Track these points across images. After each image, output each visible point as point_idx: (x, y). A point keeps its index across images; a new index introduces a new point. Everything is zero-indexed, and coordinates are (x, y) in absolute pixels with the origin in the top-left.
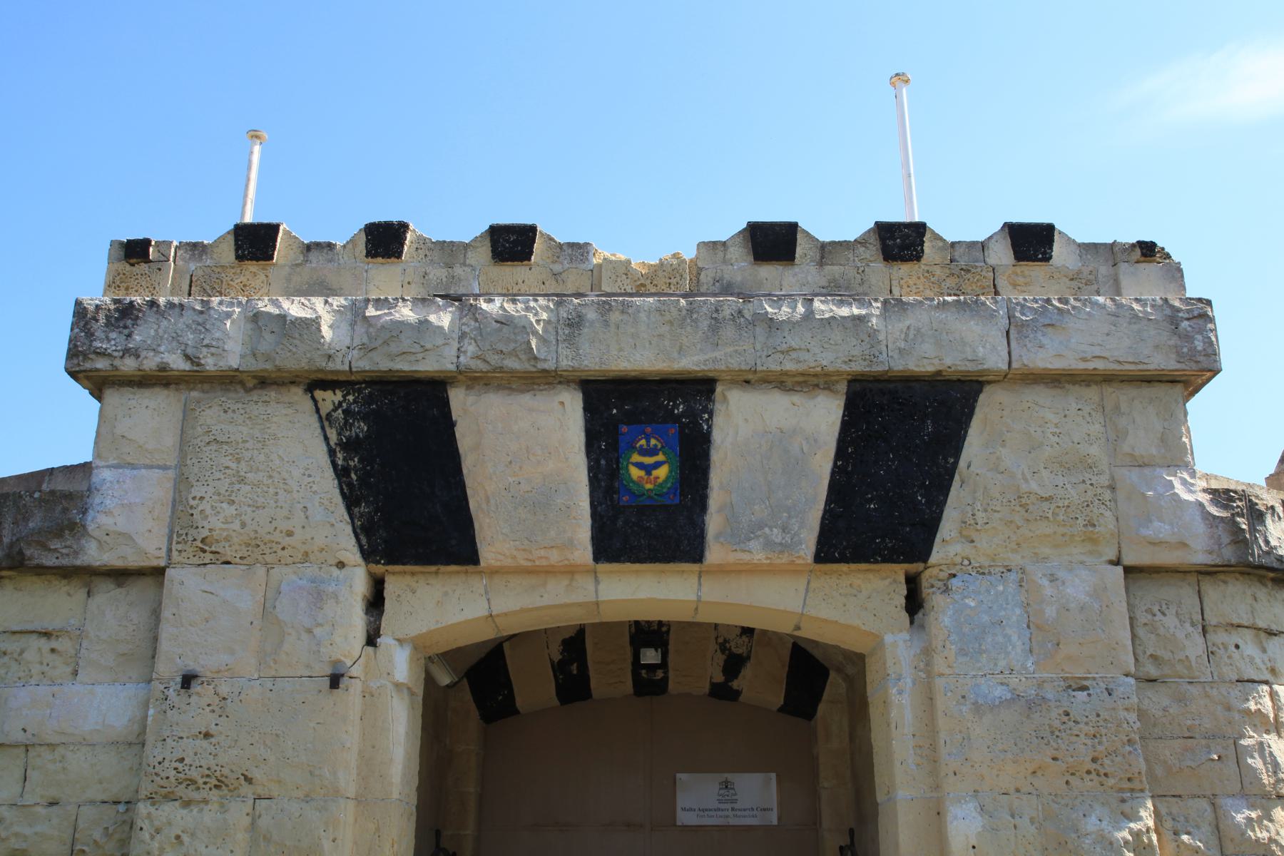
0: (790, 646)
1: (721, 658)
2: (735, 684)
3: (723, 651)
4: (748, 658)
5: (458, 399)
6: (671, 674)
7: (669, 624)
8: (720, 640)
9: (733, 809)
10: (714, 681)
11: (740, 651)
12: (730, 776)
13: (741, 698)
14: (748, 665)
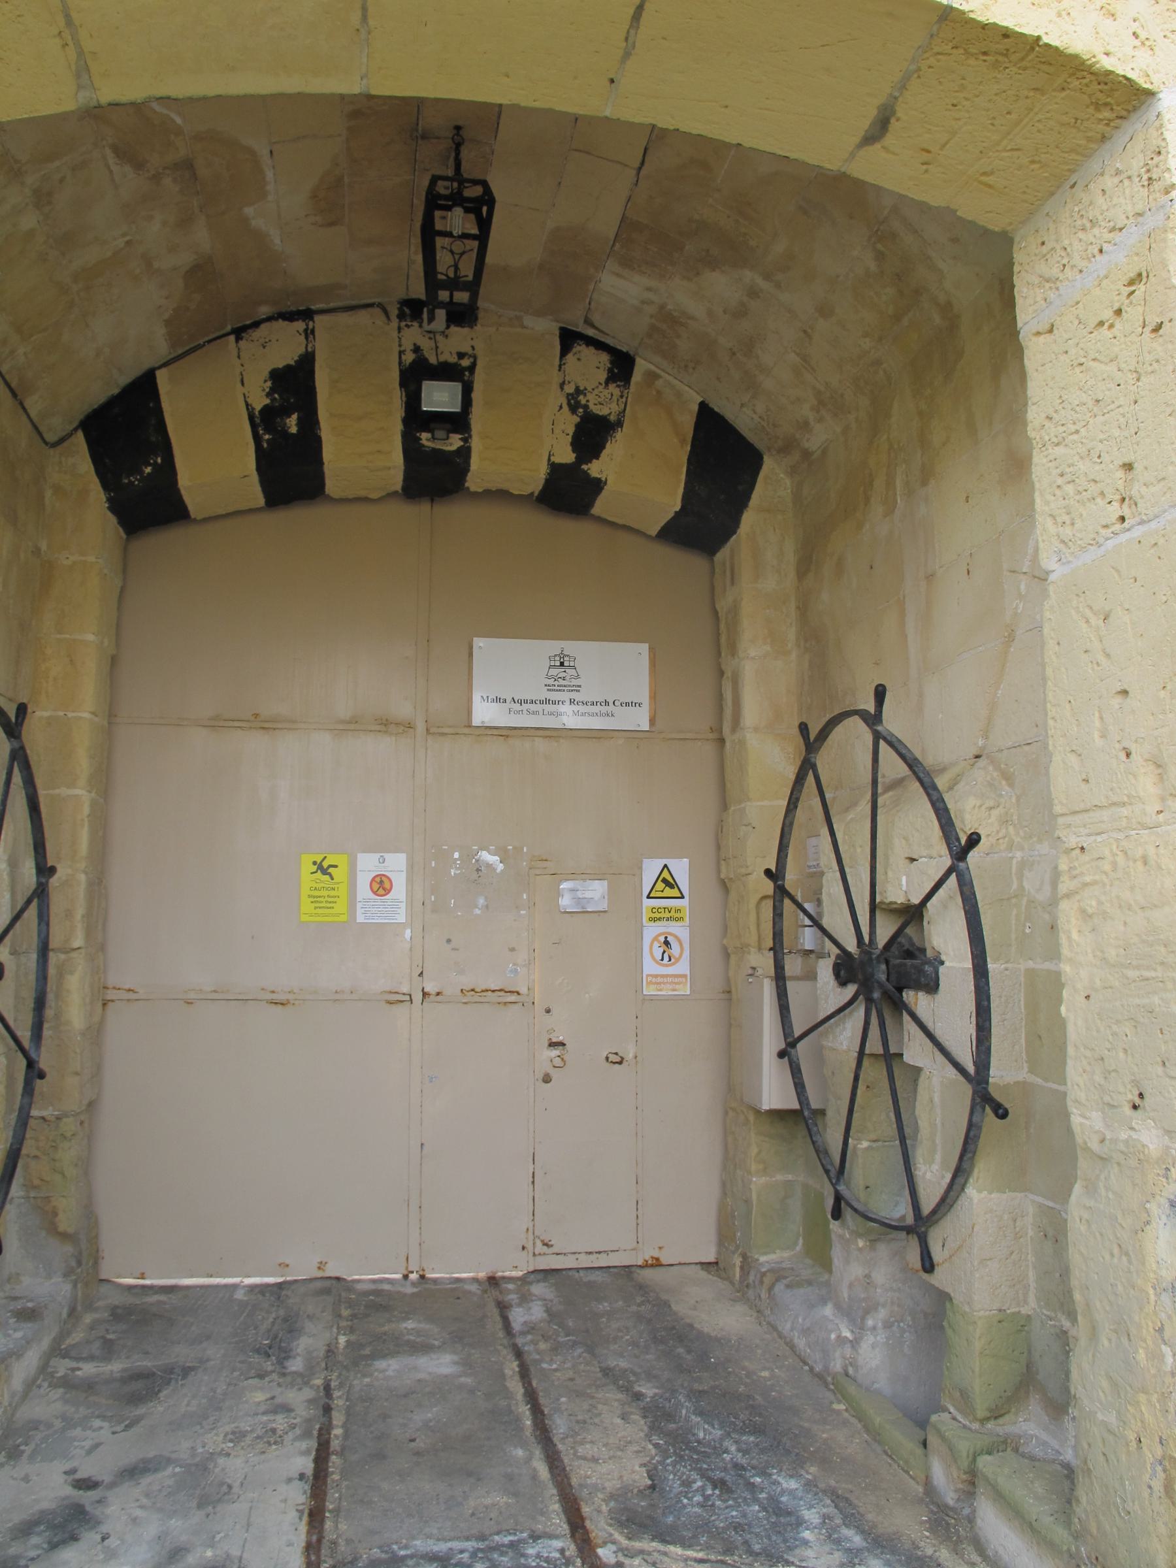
0: (696, 408)
1: (569, 422)
2: (594, 469)
3: (573, 409)
4: (619, 424)
5: (261, 501)
6: (476, 444)
7: (492, 116)
8: (570, 389)
9: (572, 702)
10: (558, 459)
11: (602, 411)
12: (570, 647)
13: (599, 507)
14: (619, 435)
